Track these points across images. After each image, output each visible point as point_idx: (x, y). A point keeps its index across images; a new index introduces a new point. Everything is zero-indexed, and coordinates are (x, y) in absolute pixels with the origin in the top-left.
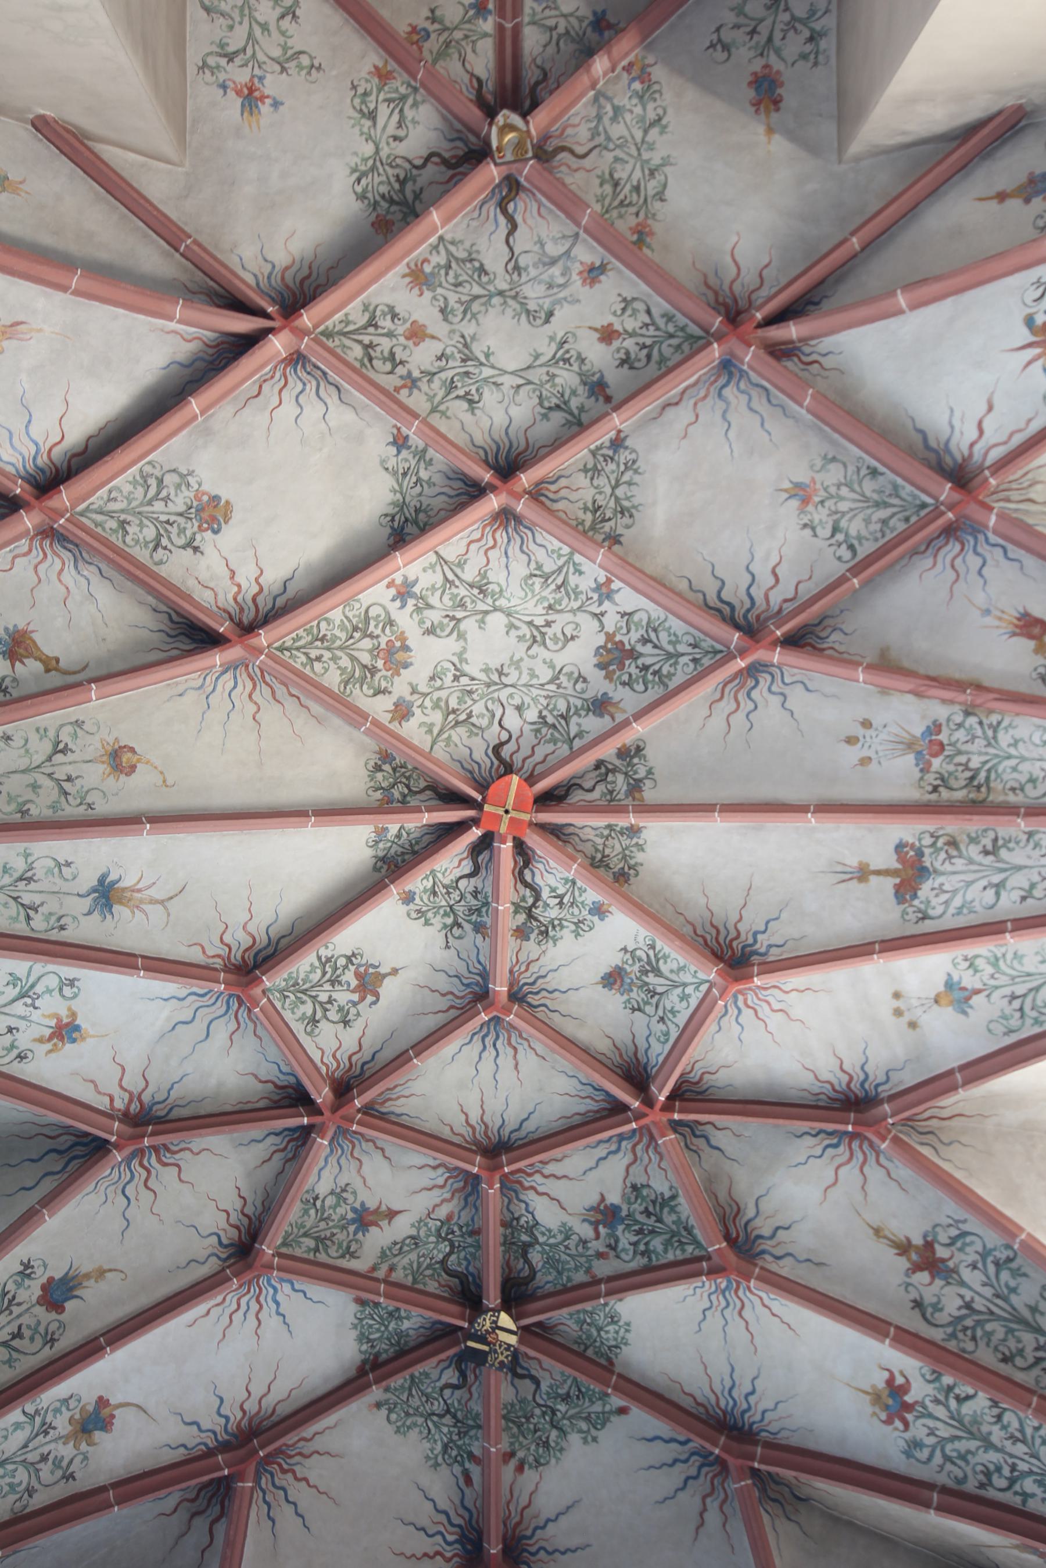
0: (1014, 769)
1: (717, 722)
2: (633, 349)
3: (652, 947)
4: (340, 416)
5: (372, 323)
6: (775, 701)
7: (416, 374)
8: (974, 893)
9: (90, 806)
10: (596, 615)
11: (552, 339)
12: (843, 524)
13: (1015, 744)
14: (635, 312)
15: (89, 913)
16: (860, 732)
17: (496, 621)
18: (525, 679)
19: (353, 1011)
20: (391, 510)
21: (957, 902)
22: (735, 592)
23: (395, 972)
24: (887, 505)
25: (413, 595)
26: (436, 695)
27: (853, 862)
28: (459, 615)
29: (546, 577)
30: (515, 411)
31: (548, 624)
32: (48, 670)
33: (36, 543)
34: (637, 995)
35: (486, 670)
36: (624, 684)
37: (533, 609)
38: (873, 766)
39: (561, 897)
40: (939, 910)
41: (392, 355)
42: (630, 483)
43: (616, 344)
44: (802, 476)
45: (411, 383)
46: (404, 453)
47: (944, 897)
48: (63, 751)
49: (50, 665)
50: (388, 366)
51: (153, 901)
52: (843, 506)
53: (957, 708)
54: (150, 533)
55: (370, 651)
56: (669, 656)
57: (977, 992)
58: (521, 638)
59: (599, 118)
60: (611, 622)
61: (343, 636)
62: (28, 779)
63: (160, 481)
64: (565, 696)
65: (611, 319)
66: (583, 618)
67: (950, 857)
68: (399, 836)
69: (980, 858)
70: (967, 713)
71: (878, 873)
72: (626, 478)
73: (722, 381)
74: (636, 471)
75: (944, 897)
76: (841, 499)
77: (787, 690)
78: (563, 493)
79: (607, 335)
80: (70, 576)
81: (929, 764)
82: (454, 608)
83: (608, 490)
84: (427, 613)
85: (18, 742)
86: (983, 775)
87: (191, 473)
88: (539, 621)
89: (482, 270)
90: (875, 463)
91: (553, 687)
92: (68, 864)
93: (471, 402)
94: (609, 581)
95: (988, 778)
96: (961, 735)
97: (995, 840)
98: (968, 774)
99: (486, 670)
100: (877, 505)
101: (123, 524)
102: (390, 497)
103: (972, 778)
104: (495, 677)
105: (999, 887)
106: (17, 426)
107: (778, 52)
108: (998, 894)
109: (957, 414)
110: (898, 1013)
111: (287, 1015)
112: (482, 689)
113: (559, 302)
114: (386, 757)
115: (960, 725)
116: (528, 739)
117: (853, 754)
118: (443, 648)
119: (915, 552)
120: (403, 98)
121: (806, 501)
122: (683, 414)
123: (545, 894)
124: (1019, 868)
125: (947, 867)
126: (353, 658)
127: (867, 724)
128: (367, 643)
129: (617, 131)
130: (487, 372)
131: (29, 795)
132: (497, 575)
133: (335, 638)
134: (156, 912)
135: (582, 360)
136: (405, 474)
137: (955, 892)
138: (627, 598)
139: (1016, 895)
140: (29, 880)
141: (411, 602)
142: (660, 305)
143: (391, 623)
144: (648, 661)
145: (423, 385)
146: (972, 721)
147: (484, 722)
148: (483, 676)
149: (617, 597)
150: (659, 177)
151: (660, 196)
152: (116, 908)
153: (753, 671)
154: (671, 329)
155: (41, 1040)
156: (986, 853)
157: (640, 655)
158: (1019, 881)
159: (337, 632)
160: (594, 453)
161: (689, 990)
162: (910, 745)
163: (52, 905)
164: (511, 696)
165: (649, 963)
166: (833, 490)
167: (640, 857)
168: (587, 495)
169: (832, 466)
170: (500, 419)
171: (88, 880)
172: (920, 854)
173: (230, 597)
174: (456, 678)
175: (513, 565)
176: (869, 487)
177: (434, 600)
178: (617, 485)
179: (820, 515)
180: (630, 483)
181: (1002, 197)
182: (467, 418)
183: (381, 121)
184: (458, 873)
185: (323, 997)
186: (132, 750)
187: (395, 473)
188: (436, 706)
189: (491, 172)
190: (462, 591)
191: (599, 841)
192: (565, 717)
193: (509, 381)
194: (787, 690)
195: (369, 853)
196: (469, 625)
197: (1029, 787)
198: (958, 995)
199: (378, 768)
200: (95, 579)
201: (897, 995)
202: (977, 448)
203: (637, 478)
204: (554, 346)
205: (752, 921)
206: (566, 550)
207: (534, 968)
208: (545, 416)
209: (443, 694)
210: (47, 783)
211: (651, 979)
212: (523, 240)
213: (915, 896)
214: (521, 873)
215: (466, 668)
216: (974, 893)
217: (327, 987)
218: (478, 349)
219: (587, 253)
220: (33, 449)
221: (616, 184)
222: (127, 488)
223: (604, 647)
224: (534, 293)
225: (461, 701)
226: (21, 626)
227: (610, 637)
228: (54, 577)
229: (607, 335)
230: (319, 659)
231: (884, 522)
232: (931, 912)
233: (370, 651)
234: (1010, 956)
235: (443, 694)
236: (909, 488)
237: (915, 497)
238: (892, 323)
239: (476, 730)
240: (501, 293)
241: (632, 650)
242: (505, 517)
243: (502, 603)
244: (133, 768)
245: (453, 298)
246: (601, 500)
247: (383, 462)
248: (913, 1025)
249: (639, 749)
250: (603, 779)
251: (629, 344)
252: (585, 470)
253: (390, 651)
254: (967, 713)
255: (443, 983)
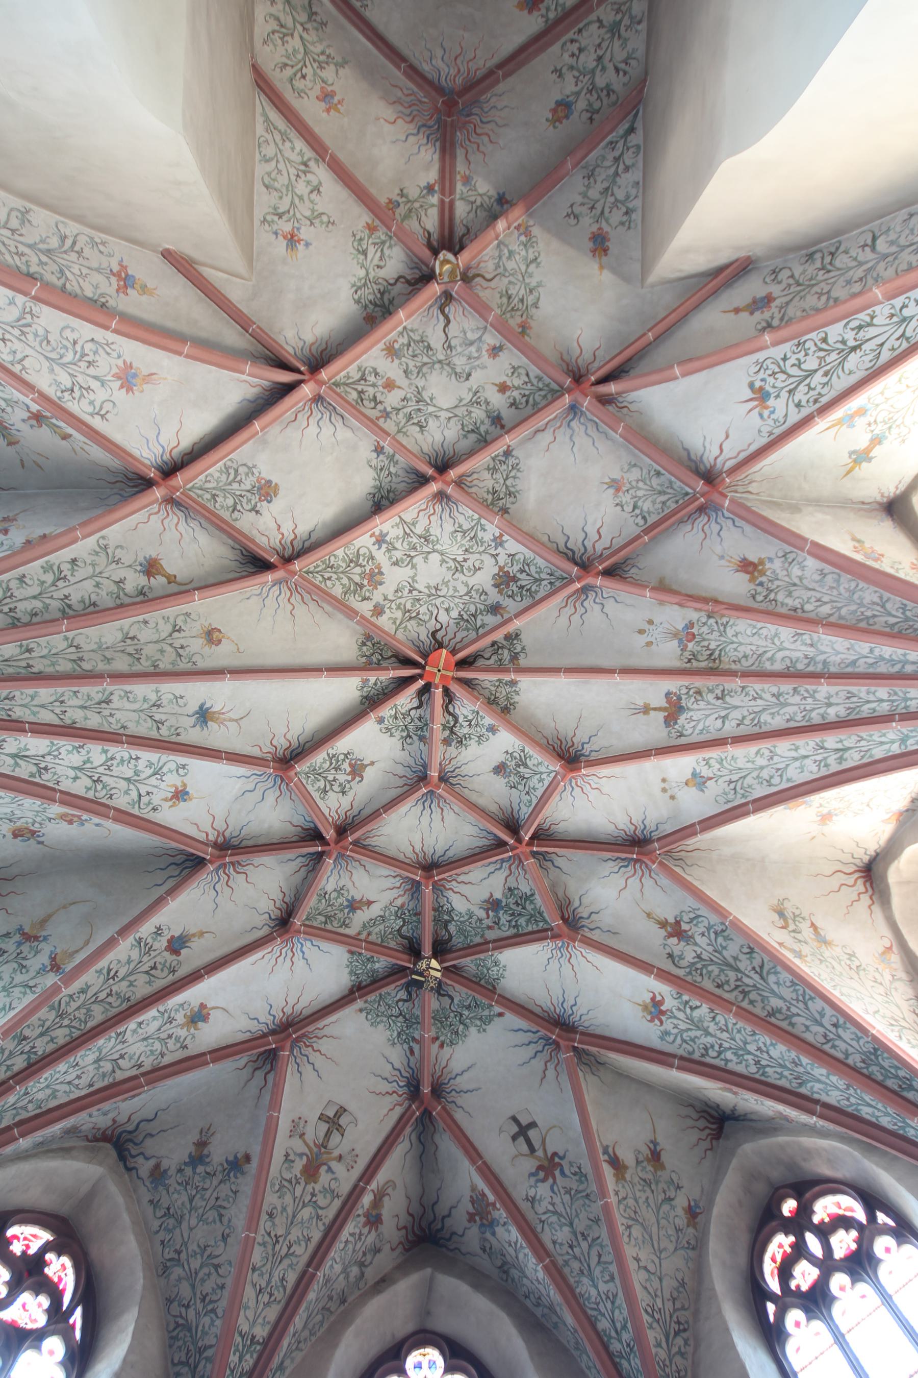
0: (735, 650)
1: (564, 620)
2: (518, 397)
3: (523, 751)
4: (343, 433)
5: (363, 378)
6: (597, 608)
7: (389, 409)
8: (710, 721)
9: (194, 663)
10: (493, 555)
11: (470, 390)
12: (640, 504)
13: (736, 635)
14: (519, 376)
15: (194, 726)
16: (646, 626)
17: (435, 558)
18: (451, 592)
19: (348, 786)
20: (373, 491)
21: (700, 726)
22: (575, 543)
23: (372, 763)
24: (665, 493)
25: (384, 542)
26: (398, 601)
27: (641, 703)
28: (413, 554)
29: (464, 532)
30: (447, 433)
31: (465, 560)
32: (169, 583)
33: (163, 506)
34: (513, 779)
35: (428, 587)
36: (509, 596)
37: (457, 552)
38: (654, 647)
39: (470, 721)
40: (690, 731)
41: (375, 397)
42: (514, 477)
43: (508, 393)
44: (616, 475)
45: (386, 415)
46: (381, 457)
47: (693, 724)
48: (179, 631)
49: (171, 579)
50: (373, 404)
51: (231, 720)
52: (640, 493)
53: (703, 614)
54: (230, 502)
55: (360, 575)
56: (536, 580)
57: (710, 779)
58: (449, 569)
59: (500, 257)
60: (502, 559)
61: (344, 565)
62: (158, 646)
63: (236, 471)
64: (474, 603)
65: (504, 378)
66: (485, 557)
67: (697, 701)
68: (375, 684)
69: (714, 701)
70: (709, 617)
71: (655, 709)
72: (512, 474)
73: (570, 417)
74: (518, 470)
75: (693, 724)
76: (639, 489)
77: (604, 602)
78: (475, 482)
79: (503, 388)
80: (182, 526)
81: (686, 646)
82: (409, 550)
83: (502, 481)
84: (394, 552)
85: (152, 625)
86: (717, 652)
87: (254, 466)
88: (460, 559)
89: (429, 347)
90: (659, 468)
91: (467, 598)
92: (181, 697)
93: (421, 427)
94: (501, 535)
95: (720, 655)
96: (705, 629)
97: (723, 691)
98: (709, 652)
99: (428, 587)
100: (660, 493)
101: (214, 496)
102: (372, 483)
103: (711, 655)
104: (433, 591)
105: (724, 718)
106: (152, 436)
107: (607, 221)
108: (723, 722)
109: (708, 440)
110: (664, 790)
111: (309, 788)
112: (425, 598)
113: (474, 368)
114: (368, 637)
115: (704, 624)
116: (452, 628)
117: (643, 639)
118: (401, 575)
119: (681, 521)
120: (383, 243)
121: (618, 490)
122: (547, 437)
123: (461, 719)
124: (736, 707)
125: (695, 706)
126: (350, 579)
127: (651, 622)
128: (358, 570)
129: (511, 265)
130: (431, 409)
131: (158, 656)
132: (435, 531)
133: (340, 566)
134: (233, 726)
135: (488, 403)
136: (381, 469)
137: (699, 721)
138: (512, 546)
139: (734, 723)
140: (159, 706)
141: (384, 546)
142: (534, 371)
143: (372, 558)
144: (524, 583)
145: (393, 416)
146: (712, 621)
147: (427, 618)
148: (426, 591)
149: (506, 545)
150: (535, 294)
151: (536, 305)
152: (210, 723)
153: (585, 590)
154: (541, 385)
155: (166, 800)
156: (718, 698)
157: (519, 579)
158: (736, 714)
159: (340, 563)
160: (494, 459)
161: (544, 776)
162: (675, 635)
163: (172, 721)
164: (443, 602)
165: (521, 760)
166: (634, 483)
167: (516, 698)
168: (490, 484)
169: (634, 469)
170: (438, 438)
171: (193, 707)
172: (679, 698)
173: (277, 541)
174: (410, 592)
175: (445, 525)
176: (655, 482)
177: (398, 545)
178: (507, 478)
179: (626, 498)
180: (514, 477)
181: (737, 311)
182: (419, 436)
183: (370, 256)
184: (410, 706)
185: (331, 778)
186: (219, 631)
187: (376, 469)
188: (398, 608)
189: (435, 289)
190: (415, 540)
191: (493, 689)
192: (474, 616)
193: (444, 415)
194: (604, 602)
195: (358, 693)
196: (418, 560)
197: (743, 661)
198: (699, 780)
199: (364, 644)
200: (198, 529)
201: (664, 780)
202: (719, 460)
203: (519, 474)
204: (471, 395)
205: (581, 736)
206: (476, 516)
207: (454, 762)
208: (465, 436)
209: (403, 601)
210: (169, 649)
211: (522, 769)
212: (453, 330)
213: (676, 723)
214: (447, 707)
215: (416, 586)
216: (710, 721)
217: (333, 771)
218: (426, 395)
219: (492, 338)
220: (161, 450)
221: (509, 298)
222: (217, 475)
223: (498, 574)
224: (459, 362)
225: (413, 605)
226: (154, 556)
227: (501, 569)
228: (173, 527)
229: (503, 388)
230: (329, 579)
231: (664, 503)
232: (685, 732)
233: (360, 575)
234: (729, 758)
235: (403, 601)
236: (679, 483)
237: (682, 489)
238: (671, 385)
239: (423, 622)
240: (440, 362)
241: (514, 576)
242: (441, 496)
243: (438, 547)
244: (220, 641)
245: (411, 364)
246: (497, 487)
247: (369, 462)
248: (672, 797)
249: (517, 635)
250: (496, 652)
251: (516, 394)
252: (488, 469)
253: (372, 575)
254: (709, 617)
255: (400, 770)
